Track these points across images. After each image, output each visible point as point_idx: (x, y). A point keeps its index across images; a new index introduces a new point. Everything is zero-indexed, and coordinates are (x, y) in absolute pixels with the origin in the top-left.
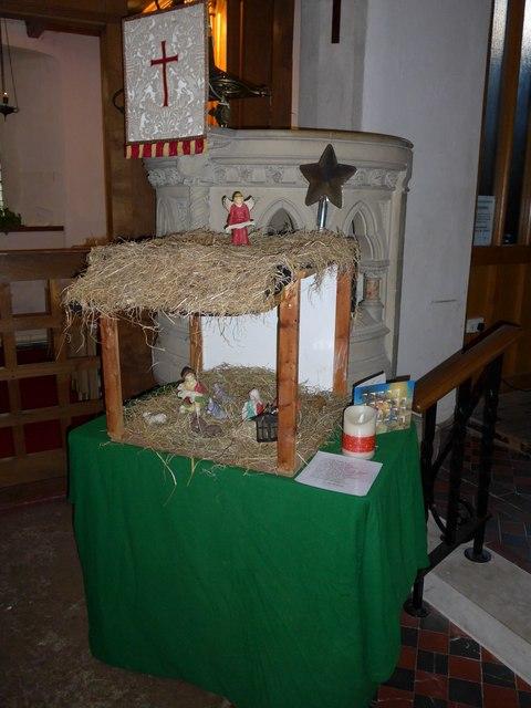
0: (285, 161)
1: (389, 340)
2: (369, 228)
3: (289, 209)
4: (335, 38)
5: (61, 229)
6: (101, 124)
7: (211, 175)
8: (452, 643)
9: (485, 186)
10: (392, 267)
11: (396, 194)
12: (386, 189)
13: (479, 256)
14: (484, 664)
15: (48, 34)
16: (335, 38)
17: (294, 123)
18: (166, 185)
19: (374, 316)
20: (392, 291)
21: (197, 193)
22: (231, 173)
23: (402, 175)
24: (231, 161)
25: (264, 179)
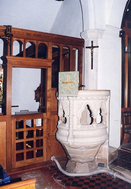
1: (108, 129)
4: (92, 68)
5: (18, 106)
10: (108, 114)
11: (108, 100)
16: (92, 68)
23: (109, 96)
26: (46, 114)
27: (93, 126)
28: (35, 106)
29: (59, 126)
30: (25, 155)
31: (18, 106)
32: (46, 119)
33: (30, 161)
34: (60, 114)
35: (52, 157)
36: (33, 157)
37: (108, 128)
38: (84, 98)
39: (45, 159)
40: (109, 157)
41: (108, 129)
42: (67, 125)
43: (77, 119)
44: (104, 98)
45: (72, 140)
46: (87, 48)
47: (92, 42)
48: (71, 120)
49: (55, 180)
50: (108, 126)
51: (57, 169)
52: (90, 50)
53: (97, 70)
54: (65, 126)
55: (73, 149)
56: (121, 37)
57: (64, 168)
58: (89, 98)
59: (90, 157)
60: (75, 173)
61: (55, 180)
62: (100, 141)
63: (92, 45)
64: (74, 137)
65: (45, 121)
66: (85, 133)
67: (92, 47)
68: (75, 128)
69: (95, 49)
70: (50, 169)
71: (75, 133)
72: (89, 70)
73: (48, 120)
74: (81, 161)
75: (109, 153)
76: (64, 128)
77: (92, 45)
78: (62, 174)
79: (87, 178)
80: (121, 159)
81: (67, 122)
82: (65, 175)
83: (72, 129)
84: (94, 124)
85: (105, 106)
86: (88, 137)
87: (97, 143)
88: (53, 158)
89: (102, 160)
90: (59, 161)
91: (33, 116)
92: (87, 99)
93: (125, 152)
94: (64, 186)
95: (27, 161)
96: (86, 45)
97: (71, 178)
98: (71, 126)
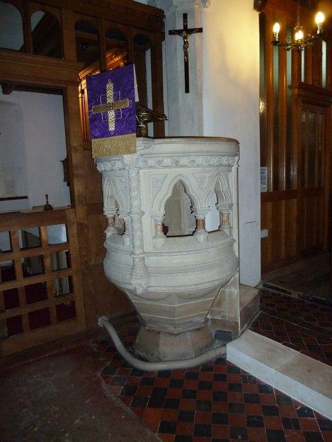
0: (181, 154)
1: (236, 245)
2: (223, 188)
3: (185, 180)
4: (187, 91)
5: (26, 197)
6: (273, 386)
7: (141, 164)
8: (297, 410)
9: (263, 163)
10: (235, 207)
11: (234, 169)
12: (230, 166)
13: (265, 198)
14: (319, 420)
15: (14, 92)
16: (187, 91)
17: (166, 135)
18: (112, 170)
19: (228, 234)
20: (236, 221)
21: (133, 174)
22: (151, 162)
23: (237, 158)
24: (152, 156)
25: (170, 164)
26: (75, 212)
27: (196, 239)
28: (60, 198)
29: (108, 244)
30: (25, 321)
31: (26, 197)
32: (76, 226)
33: (41, 334)
34: (109, 210)
35: (100, 320)
36: (48, 323)
37: (237, 242)
38: (167, 161)
39: (78, 326)
40: (241, 317)
41: (236, 245)
42: (127, 239)
43: (153, 223)
44: (224, 161)
45: (143, 282)
46: (171, 33)
47: (185, 16)
48: (136, 225)
49: (104, 385)
50: (235, 237)
51: (114, 349)
52: (179, 40)
53: (199, 96)
54: (123, 243)
55: (149, 302)
56: (258, 10)
57: (128, 345)
58: (184, 161)
59: (196, 320)
60: (160, 361)
61: (104, 385)
62: (219, 280)
63: (185, 26)
64: (148, 272)
65: (74, 230)
66: (177, 260)
67: (187, 31)
68: (148, 248)
69: (191, 38)
70: (96, 350)
71: (151, 261)
72: (180, 97)
73: (80, 225)
74: (172, 329)
75: (241, 304)
76: (121, 247)
77: (185, 26)
78: (126, 364)
79: (191, 373)
80: (268, 314)
81: (127, 232)
82: (132, 366)
83: (141, 251)
84: (201, 236)
85: (228, 184)
86: (185, 270)
87: (210, 285)
88: (102, 321)
89: (223, 323)
90: (116, 327)
91: (49, 214)
92: (177, 164)
93: (274, 294)
94: (129, 410)
95: (32, 337)
96: (168, 28)
97: (147, 377)
98: (137, 243)
